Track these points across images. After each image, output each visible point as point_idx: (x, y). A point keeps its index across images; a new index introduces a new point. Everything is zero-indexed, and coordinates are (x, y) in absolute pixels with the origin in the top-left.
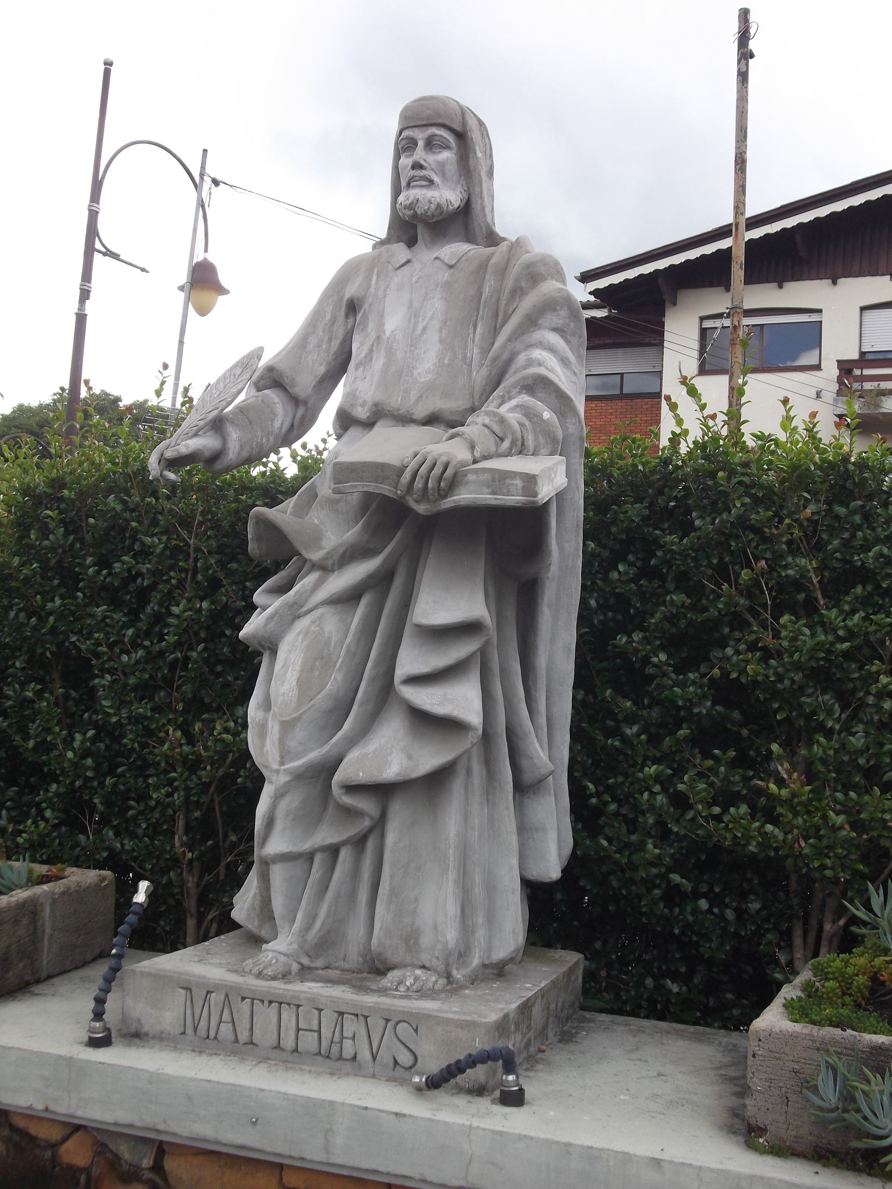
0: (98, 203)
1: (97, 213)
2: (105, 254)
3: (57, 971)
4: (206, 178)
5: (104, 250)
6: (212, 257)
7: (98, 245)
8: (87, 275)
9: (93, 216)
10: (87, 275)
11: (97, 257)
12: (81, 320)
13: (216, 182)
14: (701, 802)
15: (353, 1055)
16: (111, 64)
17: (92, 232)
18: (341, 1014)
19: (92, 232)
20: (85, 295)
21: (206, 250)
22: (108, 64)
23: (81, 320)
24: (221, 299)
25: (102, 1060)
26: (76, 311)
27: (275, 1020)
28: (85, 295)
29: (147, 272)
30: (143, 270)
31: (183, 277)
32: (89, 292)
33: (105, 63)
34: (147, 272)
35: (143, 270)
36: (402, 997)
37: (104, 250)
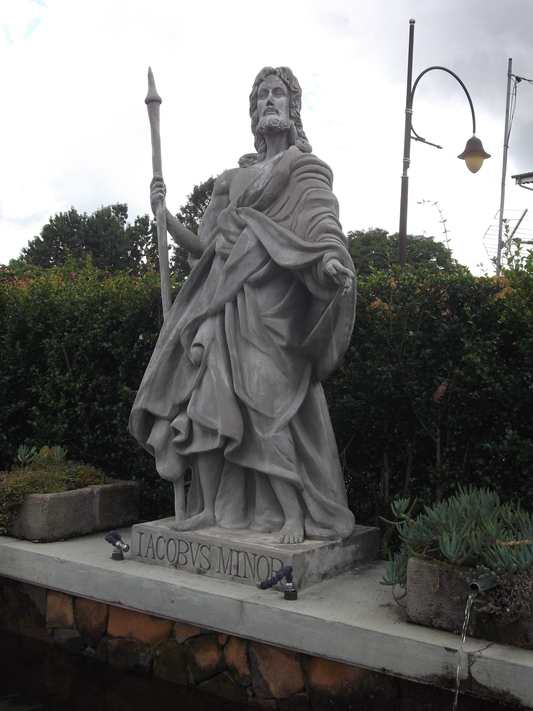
0: (411, 108)
1: (411, 114)
2: (416, 139)
3: (88, 530)
4: (512, 77)
5: (416, 137)
6: (478, 136)
7: (412, 134)
8: (407, 153)
9: (409, 116)
10: (407, 153)
11: (412, 141)
12: (405, 181)
13: (518, 79)
14: (498, 446)
15: (387, 609)
16: (414, 22)
17: (409, 127)
18: (231, 550)
19: (409, 127)
20: (406, 165)
21: (474, 132)
22: (412, 22)
23: (405, 181)
24: (485, 161)
25: (63, 557)
26: (402, 175)
27: (138, 540)
28: (406, 165)
29: (441, 148)
30: (439, 147)
31: (462, 149)
32: (409, 163)
33: (410, 22)
34: (441, 148)
35: (439, 147)
36: (285, 547)
37: (416, 137)
